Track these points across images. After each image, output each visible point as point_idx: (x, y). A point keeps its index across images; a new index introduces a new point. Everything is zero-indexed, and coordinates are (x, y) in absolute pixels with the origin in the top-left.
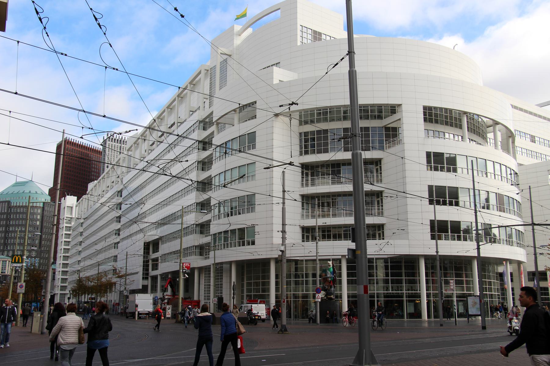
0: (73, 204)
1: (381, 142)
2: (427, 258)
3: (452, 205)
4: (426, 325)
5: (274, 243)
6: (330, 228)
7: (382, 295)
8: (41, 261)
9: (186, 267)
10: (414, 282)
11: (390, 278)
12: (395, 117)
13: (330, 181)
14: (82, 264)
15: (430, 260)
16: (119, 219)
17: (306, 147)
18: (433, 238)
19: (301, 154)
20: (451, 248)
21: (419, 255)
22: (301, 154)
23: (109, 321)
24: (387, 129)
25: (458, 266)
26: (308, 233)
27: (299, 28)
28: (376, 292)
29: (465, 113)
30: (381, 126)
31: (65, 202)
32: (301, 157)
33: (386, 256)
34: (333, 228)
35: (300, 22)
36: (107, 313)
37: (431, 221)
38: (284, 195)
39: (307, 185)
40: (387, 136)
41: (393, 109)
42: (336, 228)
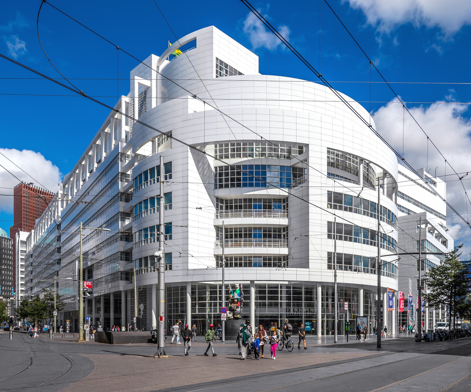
0: (436, 186)
1: (289, 180)
2: (325, 286)
5: (190, 268)
6: (251, 257)
7: (285, 316)
8: (3, 288)
9: (87, 286)
10: (311, 305)
11: (292, 301)
13: (242, 213)
14: (162, 314)
15: (326, 287)
16: (59, 238)
17: (221, 181)
18: (329, 267)
20: (347, 277)
21: (316, 282)
24: (294, 168)
25: (348, 293)
26: (225, 262)
27: (215, 60)
28: (279, 313)
30: (289, 165)
33: (287, 283)
34: (254, 257)
35: (216, 54)
37: (329, 254)
40: (295, 176)
42: (256, 257)
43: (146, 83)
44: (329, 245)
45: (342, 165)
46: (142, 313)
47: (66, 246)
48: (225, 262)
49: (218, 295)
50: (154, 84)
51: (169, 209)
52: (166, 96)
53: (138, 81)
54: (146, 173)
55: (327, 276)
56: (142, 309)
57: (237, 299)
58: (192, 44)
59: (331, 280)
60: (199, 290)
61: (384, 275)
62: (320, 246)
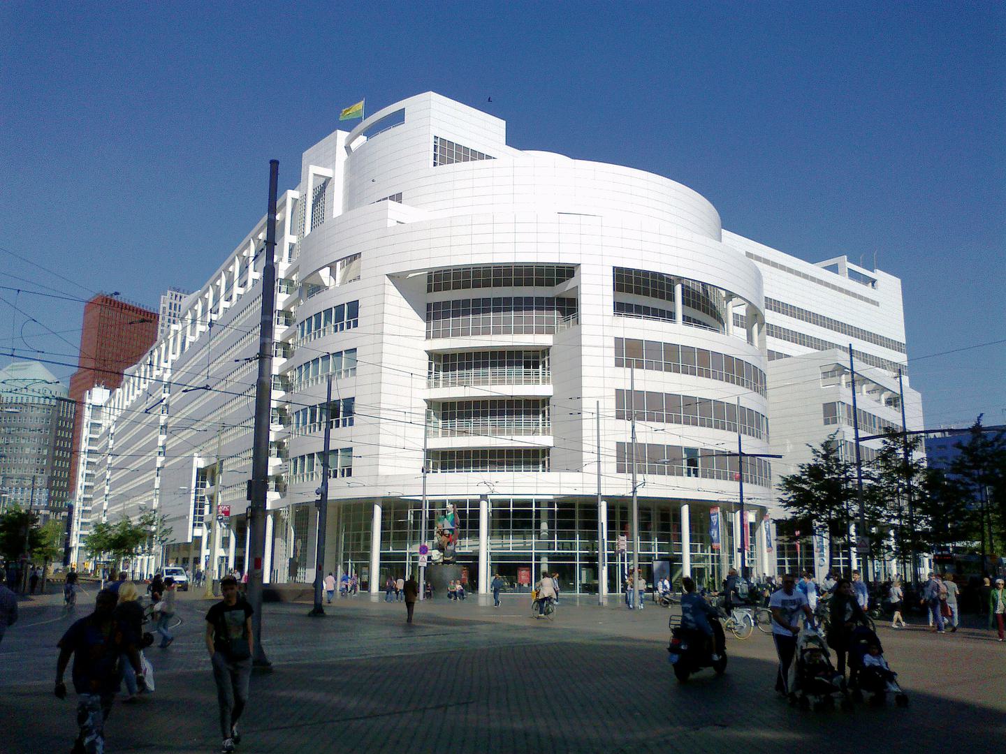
3: (719, 428)
4: (605, 603)
5: (379, 474)
12: (570, 284)
15: (619, 508)
19: (428, 337)
20: (659, 486)
22: (428, 337)
23: (349, 132)
29: (680, 279)
31: (90, 398)
32: (429, 341)
33: (551, 497)
36: (151, 523)
38: (599, 458)
39: (436, 385)
41: (567, 272)
43: (326, 172)
44: (620, 431)
45: (640, 290)
46: (299, 553)
47: (529, 624)
48: (446, 460)
49: (534, 519)
50: (338, 173)
51: (350, 425)
52: (353, 199)
53: (313, 171)
54: (318, 315)
55: (618, 485)
56: (299, 548)
57: (450, 530)
58: (398, 118)
59: (627, 492)
60: (396, 509)
61: (748, 482)
62: (604, 432)
